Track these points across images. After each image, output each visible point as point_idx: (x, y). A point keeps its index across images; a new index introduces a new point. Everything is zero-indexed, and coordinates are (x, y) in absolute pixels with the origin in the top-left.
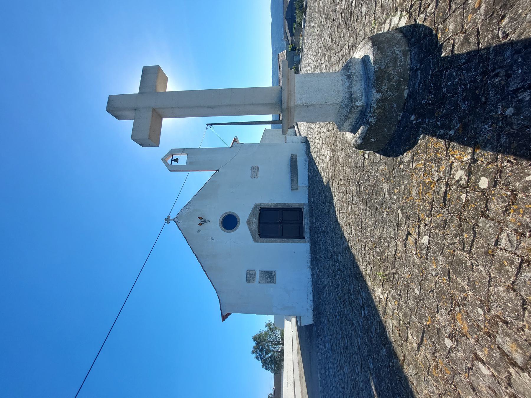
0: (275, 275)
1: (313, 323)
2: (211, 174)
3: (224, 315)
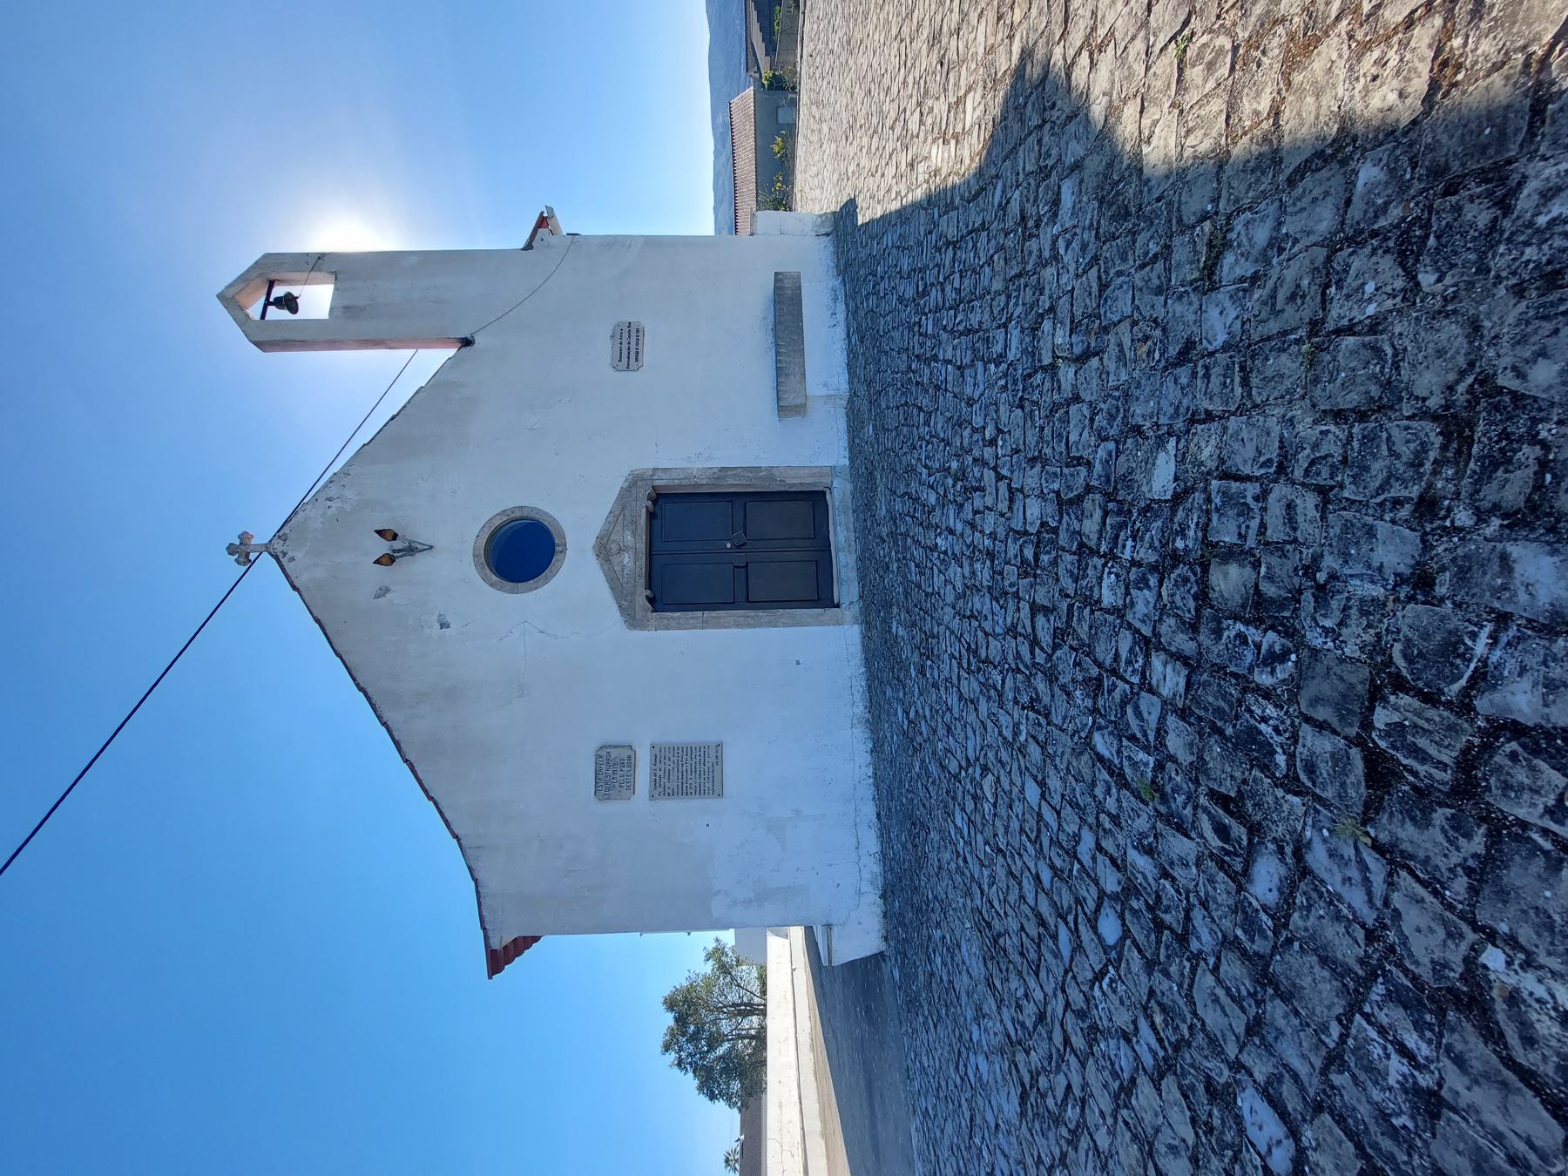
0: (719, 760)
1: (883, 947)
2: (433, 359)
3: (500, 941)
